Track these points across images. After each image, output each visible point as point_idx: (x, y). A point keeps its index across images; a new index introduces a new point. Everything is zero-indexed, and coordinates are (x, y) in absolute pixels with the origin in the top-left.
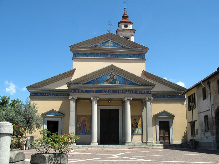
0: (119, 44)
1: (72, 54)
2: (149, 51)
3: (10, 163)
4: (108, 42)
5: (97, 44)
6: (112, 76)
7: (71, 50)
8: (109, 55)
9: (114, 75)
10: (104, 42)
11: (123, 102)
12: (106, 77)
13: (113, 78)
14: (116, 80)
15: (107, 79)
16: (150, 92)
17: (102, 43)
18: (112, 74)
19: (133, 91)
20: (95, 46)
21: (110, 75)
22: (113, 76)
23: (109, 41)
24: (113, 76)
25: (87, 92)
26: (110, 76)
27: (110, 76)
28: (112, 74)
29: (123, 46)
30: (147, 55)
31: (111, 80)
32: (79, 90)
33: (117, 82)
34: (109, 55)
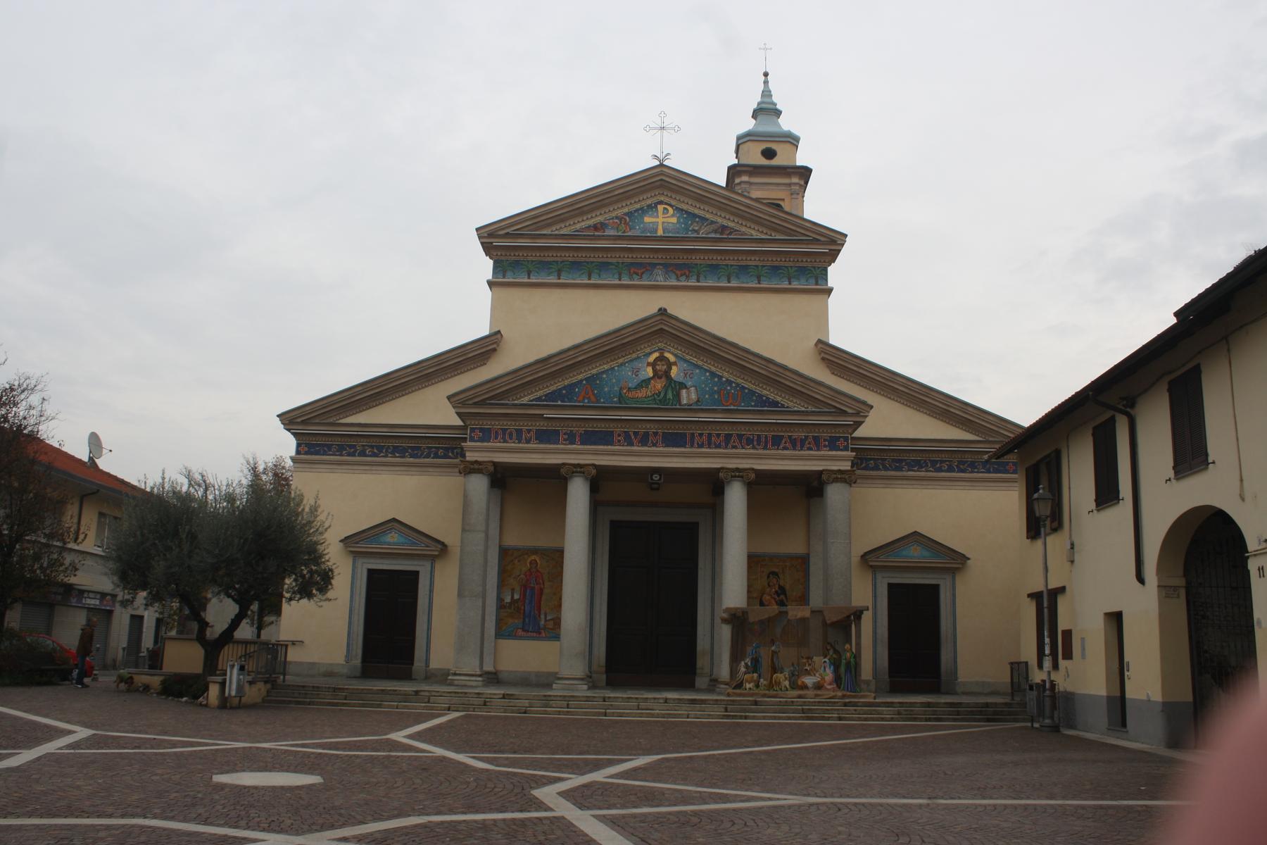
0: (708, 216)
6: (661, 367)
7: (488, 249)
9: (672, 358)
11: (715, 483)
12: (636, 372)
13: (667, 374)
14: (683, 386)
17: (629, 214)
18: (662, 358)
20: (595, 227)
22: (670, 365)
23: (661, 203)
24: (670, 365)
25: (541, 442)
26: (653, 365)
27: (653, 365)
28: (662, 358)
31: (659, 385)
32: (504, 431)
33: (684, 392)
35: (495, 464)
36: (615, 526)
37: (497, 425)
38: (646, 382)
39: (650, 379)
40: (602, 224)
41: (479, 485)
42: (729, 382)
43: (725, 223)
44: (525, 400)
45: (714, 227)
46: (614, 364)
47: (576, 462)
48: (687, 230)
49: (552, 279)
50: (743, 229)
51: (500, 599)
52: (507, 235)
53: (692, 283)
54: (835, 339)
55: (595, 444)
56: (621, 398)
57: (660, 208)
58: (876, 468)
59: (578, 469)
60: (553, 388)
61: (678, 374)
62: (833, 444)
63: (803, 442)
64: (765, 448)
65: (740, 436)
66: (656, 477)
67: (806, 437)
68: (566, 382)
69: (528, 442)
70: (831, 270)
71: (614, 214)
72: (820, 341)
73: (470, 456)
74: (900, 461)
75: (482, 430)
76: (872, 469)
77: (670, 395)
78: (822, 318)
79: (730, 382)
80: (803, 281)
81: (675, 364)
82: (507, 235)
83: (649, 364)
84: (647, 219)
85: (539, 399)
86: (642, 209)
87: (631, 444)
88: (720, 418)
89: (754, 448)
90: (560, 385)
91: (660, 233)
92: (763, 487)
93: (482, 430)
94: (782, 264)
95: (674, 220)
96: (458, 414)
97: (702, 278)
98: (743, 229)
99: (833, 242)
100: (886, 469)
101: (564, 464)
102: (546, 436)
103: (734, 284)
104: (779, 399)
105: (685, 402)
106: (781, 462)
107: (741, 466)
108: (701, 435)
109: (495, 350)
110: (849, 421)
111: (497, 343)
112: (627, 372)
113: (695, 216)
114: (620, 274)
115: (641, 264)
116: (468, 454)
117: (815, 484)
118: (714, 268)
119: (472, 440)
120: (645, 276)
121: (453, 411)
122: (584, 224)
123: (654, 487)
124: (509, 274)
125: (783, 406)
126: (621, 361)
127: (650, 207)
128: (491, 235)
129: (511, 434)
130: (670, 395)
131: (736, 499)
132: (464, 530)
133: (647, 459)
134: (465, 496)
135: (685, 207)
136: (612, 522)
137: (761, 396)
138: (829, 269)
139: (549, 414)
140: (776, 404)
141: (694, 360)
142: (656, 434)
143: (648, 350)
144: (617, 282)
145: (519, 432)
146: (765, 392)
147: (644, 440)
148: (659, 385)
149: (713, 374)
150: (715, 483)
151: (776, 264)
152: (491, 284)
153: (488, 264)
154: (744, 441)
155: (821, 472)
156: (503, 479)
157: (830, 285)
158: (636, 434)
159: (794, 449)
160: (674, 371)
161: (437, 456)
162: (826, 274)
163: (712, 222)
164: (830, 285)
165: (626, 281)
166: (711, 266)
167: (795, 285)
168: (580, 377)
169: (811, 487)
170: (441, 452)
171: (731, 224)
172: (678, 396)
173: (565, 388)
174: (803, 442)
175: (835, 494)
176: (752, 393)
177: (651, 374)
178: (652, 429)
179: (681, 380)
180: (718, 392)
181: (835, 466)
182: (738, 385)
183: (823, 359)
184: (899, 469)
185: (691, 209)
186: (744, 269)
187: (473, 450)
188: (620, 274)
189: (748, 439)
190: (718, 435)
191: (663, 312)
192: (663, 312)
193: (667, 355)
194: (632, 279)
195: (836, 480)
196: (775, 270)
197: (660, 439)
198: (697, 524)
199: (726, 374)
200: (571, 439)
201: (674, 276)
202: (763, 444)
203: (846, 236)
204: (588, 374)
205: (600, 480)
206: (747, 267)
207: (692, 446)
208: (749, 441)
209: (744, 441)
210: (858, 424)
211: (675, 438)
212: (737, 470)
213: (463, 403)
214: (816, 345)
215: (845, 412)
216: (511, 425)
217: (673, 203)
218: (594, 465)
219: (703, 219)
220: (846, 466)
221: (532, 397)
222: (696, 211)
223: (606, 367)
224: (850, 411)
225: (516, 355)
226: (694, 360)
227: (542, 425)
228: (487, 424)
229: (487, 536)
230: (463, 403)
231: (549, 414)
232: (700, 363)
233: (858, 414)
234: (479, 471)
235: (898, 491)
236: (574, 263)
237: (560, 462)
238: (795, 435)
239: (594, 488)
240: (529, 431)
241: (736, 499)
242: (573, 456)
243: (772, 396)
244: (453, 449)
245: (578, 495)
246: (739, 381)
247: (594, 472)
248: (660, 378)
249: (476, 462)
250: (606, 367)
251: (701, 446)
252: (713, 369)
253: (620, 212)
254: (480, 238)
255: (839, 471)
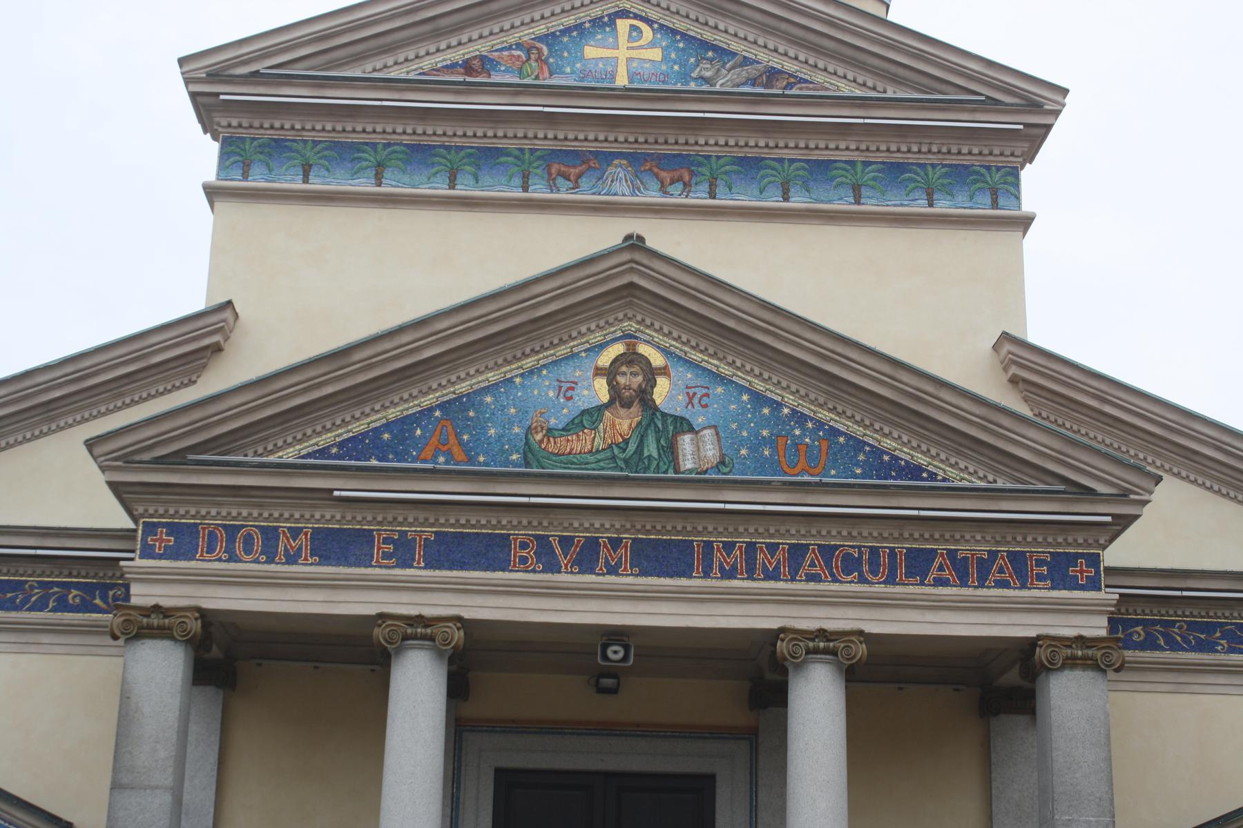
0: (735, 46)
1: (204, 155)
2: (718, 778)
3: (1159, 480)
4: (605, 23)
5: (481, 48)
6: (630, 380)
7: (207, 110)
8: (619, 172)
9: (657, 359)
10: (567, 31)
11: (758, 676)
12: (567, 390)
13: (644, 396)
14: (683, 425)
15: (567, 413)
16: (1080, 571)
17: (550, 38)
18: (631, 358)
19: (874, 551)
20: (468, 67)
21: (605, 359)
22: (651, 374)
23: (624, 14)
24: (651, 374)
25: (325, 559)
26: (610, 373)
27: (610, 373)
28: (631, 358)
29: (773, 75)
30: (1038, 183)
31: (624, 422)
32: (232, 531)
33: (686, 441)
34: (619, 172)
35: (203, 614)
36: (509, 784)
37: (213, 516)
38: (593, 415)
39: (601, 409)
40: (483, 59)
41: (161, 668)
42: (799, 418)
43: (776, 62)
44: (288, 455)
45: (746, 72)
46: (511, 370)
47: (413, 611)
48: (685, 76)
49: (364, 185)
50: (820, 78)
51: (265, 562)
52: (255, 78)
53: (699, 198)
54: (1041, 332)
55: (462, 567)
56: (528, 452)
57: (623, 25)
58: (1149, 644)
59: (418, 630)
60: (358, 427)
61: (670, 397)
62: (1060, 571)
63: (984, 567)
64: (891, 580)
65: (827, 552)
66: (615, 653)
67: (993, 555)
68: (393, 413)
69: (291, 559)
70: (1028, 175)
71: (512, 38)
72: (1006, 337)
73: (142, 595)
74: (1209, 628)
75: (173, 529)
76: (1142, 646)
77: (651, 449)
78: (1011, 283)
79: (800, 419)
80: (961, 198)
81: (664, 371)
82: (255, 78)
83: (599, 372)
84: (591, 52)
85: (323, 453)
86: (579, 27)
87: (553, 567)
88: (776, 502)
89: (862, 580)
90: (376, 420)
91: (622, 81)
92: (883, 677)
93: (173, 529)
94: (912, 159)
95: (656, 54)
96: (113, 485)
97: (721, 189)
98: (820, 78)
99: (1034, 106)
100: (1174, 646)
101: (382, 616)
102: (339, 546)
103: (798, 201)
104: (922, 460)
105: (687, 463)
106: (930, 616)
107: (831, 626)
108: (729, 547)
109: (217, 349)
110: (1102, 513)
111: (223, 330)
112: (544, 390)
113: (705, 45)
114: (525, 177)
115: (576, 154)
116: (135, 589)
117: (1012, 677)
118: (750, 166)
119: (147, 553)
120: (584, 183)
121: (100, 479)
122: (440, 60)
123: (606, 681)
124: (257, 170)
125: (933, 476)
126: (529, 363)
127: (597, 22)
128: (215, 76)
129: (248, 541)
130: (651, 449)
131: (817, 709)
132: (116, 786)
133: (593, 605)
134: (125, 696)
135: (680, 25)
136: (499, 772)
137: (877, 452)
138: (1024, 174)
139: (345, 488)
140: (915, 471)
141: (713, 364)
142: (615, 543)
143: (596, 338)
144: (519, 194)
145: (270, 535)
146: (888, 443)
147: (587, 558)
148: (624, 422)
149: (758, 399)
150: (758, 676)
151: (898, 158)
152: (213, 193)
153: (210, 149)
154: (837, 562)
155: (1033, 643)
156: (226, 658)
157: (1027, 206)
158: (566, 542)
159: (964, 584)
160: (662, 391)
161: (63, 606)
162: (1017, 185)
163: (746, 61)
164: (1027, 206)
165: (539, 192)
166: (742, 161)
167: (943, 206)
168: (428, 401)
169: (1000, 686)
170: (73, 596)
171: (790, 66)
172: (671, 451)
173: (388, 426)
174: (984, 567)
175: (1068, 696)
176: (859, 444)
177: (605, 397)
178: (604, 528)
179: (679, 411)
180: (771, 442)
181: (1066, 627)
182: (820, 424)
183: (1014, 381)
184: (1207, 646)
185: (695, 31)
186: (820, 170)
187: (151, 578)
188: (525, 177)
189: (847, 558)
190: (773, 548)
191: (634, 243)
192: (634, 243)
193: (643, 349)
194: (553, 187)
195: (1072, 663)
196: (895, 172)
197: (624, 553)
198: (711, 778)
199: (790, 399)
200: (402, 553)
201: (656, 185)
202: (884, 571)
203: (1065, 92)
204: (448, 394)
205: (476, 662)
206: (827, 165)
207: (706, 575)
208: (851, 565)
209: (837, 562)
210: (1123, 522)
211: (664, 556)
212: (822, 634)
213: (128, 459)
214: (996, 347)
215: (1090, 491)
216: (250, 517)
217: (653, 14)
218: (459, 619)
219: (723, 53)
220: (1096, 627)
221: (306, 447)
222: (708, 36)
223: (493, 376)
224: (1102, 489)
225: (271, 343)
226: (713, 364)
227: (330, 518)
228: (186, 513)
229: (178, 802)
230: (128, 459)
231: (345, 488)
232: (726, 370)
233: (1123, 496)
234: (162, 633)
235: (1207, 701)
236: (415, 148)
237: (371, 610)
238: (963, 549)
239: (458, 688)
240: (295, 533)
241: (817, 709)
242: (405, 597)
243: (904, 454)
244: (105, 588)
245: (417, 694)
246: (824, 415)
247: (458, 636)
248: (627, 405)
249: (157, 609)
250: (493, 376)
251: (730, 574)
252: (759, 386)
253: (525, 35)
254: (187, 81)
255: (1080, 640)
